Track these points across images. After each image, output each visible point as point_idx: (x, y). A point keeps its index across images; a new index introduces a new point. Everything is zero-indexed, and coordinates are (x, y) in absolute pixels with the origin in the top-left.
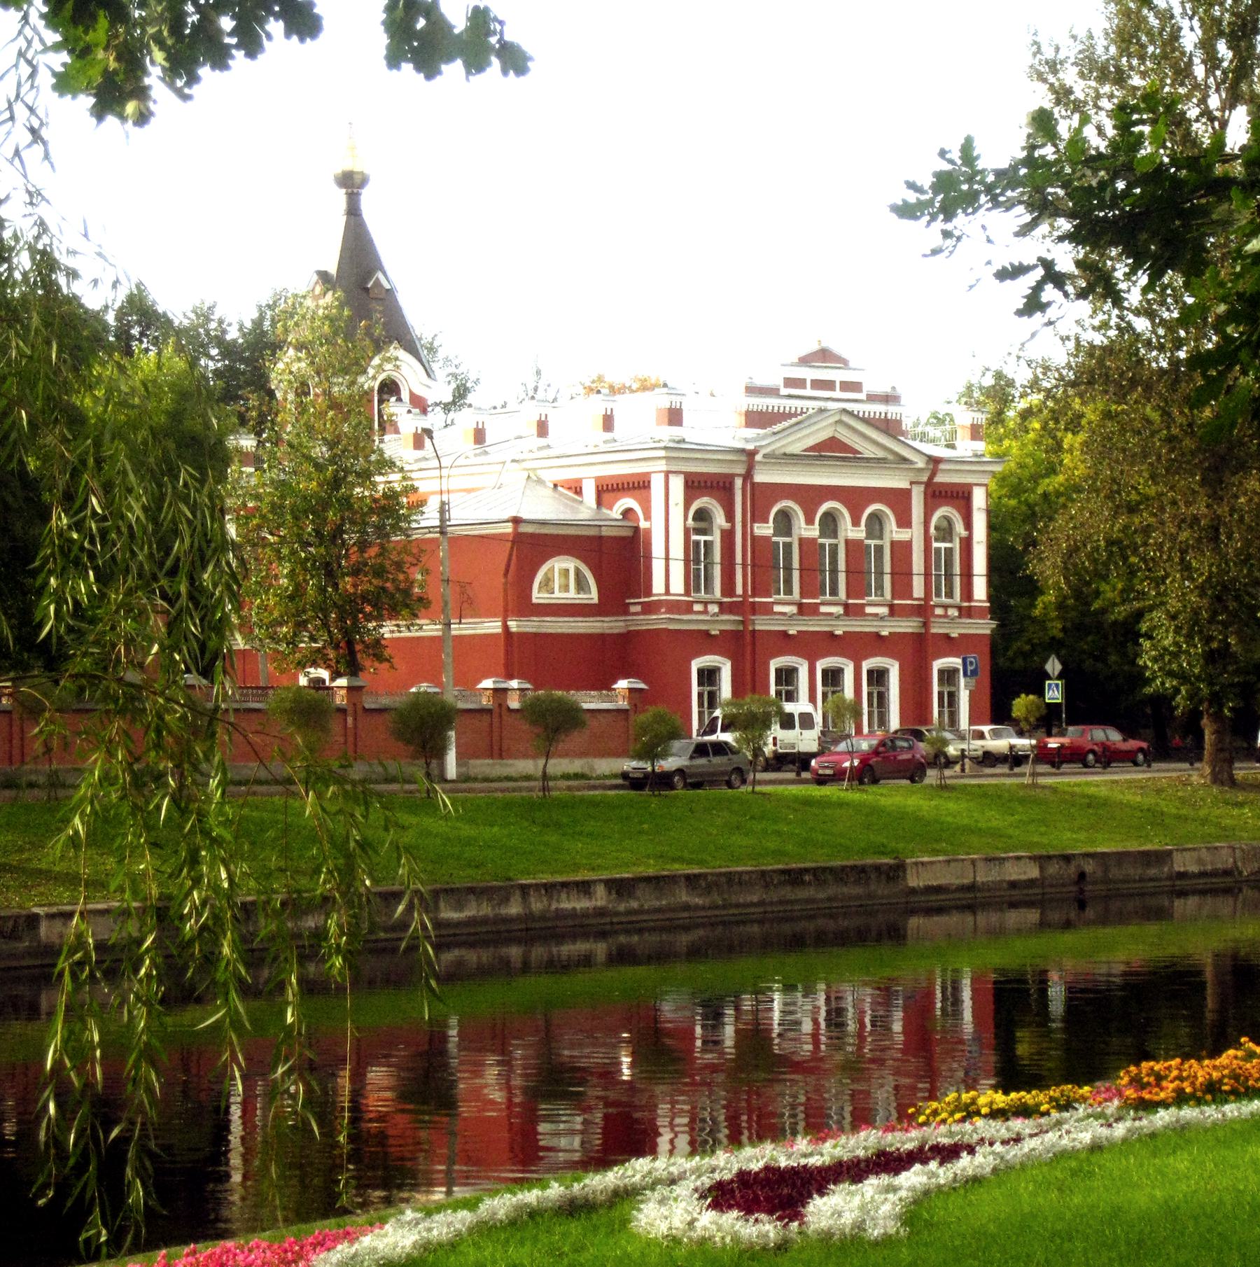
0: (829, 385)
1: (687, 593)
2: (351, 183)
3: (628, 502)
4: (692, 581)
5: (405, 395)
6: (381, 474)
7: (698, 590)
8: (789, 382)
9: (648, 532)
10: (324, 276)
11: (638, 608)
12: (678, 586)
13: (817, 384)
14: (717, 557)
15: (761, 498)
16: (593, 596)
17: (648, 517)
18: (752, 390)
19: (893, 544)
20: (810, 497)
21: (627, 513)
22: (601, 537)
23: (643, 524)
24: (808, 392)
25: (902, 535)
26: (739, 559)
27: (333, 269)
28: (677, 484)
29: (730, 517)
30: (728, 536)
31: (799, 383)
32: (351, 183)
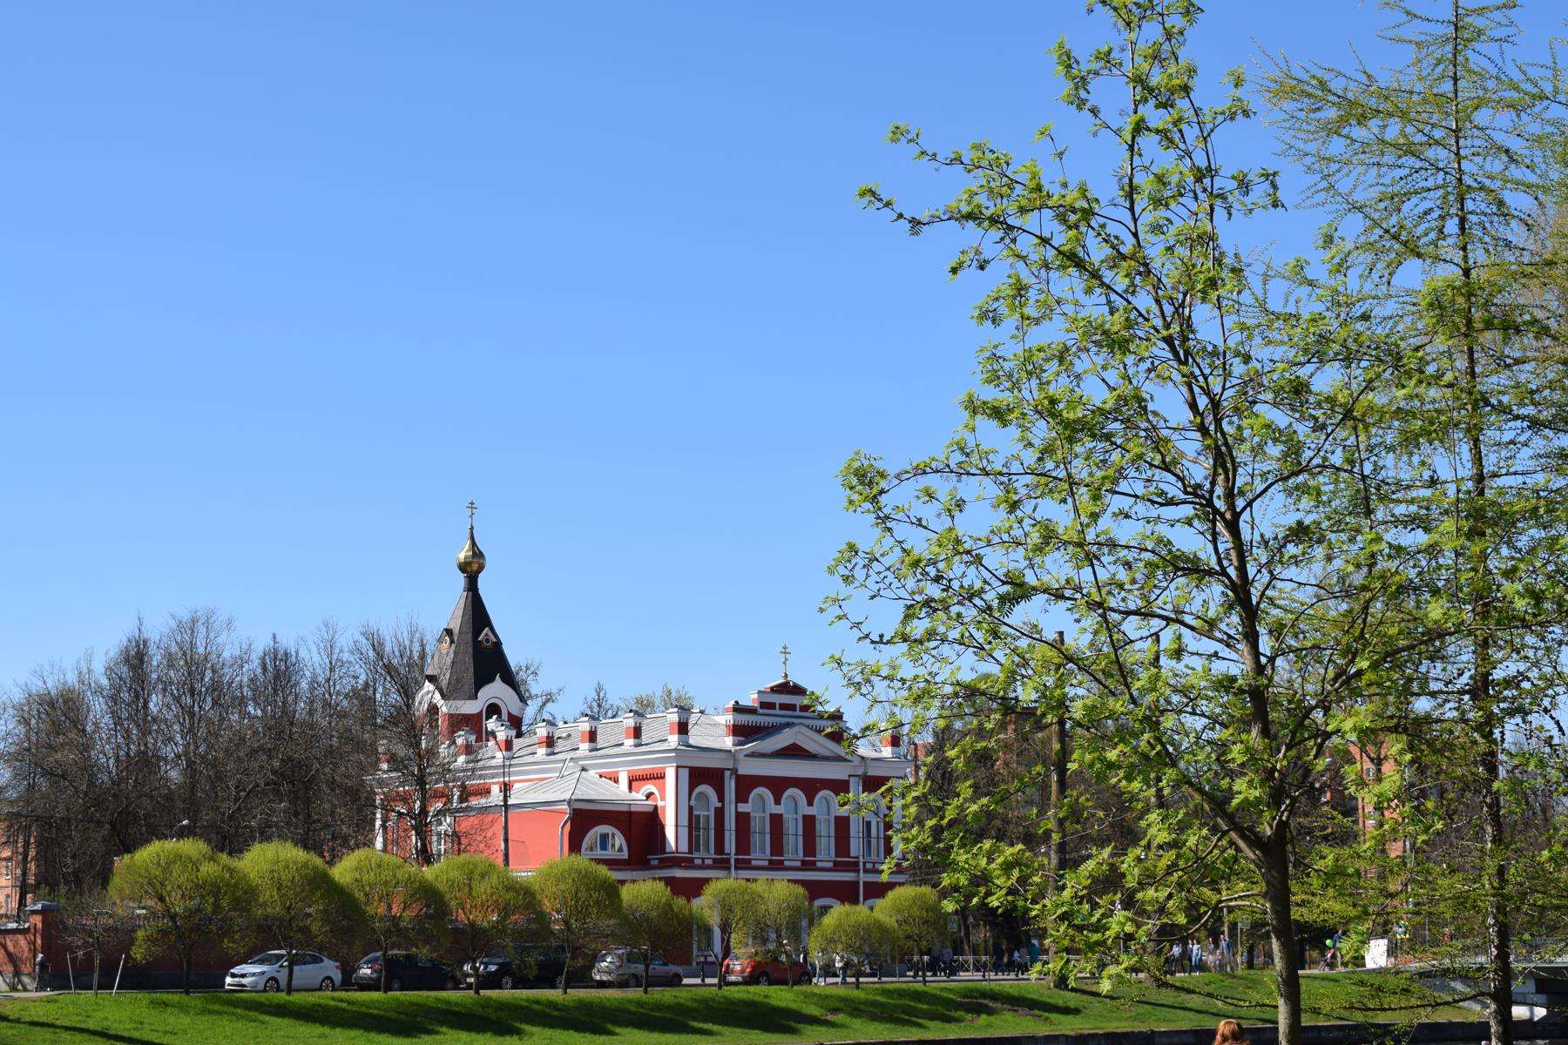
0: (792, 707)
1: (690, 852)
2: (472, 570)
3: (650, 787)
4: (693, 843)
5: (505, 716)
6: (1411, 793)
7: (698, 850)
8: (764, 705)
9: (664, 808)
10: (449, 632)
11: (655, 862)
12: (684, 847)
13: (783, 707)
14: (712, 825)
15: (746, 785)
16: (625, 855)
17: (663, 798)
18: (738, 709)
19: (805, 817)
20: (778, 786)
21: (649, 796)
22: (129, 851)
23: (660, 804)
24: (777, 711)
25: (809, 811)
26: (712, 832)
27: (455, 626)
28: (685, 773)
29: (721, 798)
30: (720, 813)
31: (771, 706)
32: (472, 570)
